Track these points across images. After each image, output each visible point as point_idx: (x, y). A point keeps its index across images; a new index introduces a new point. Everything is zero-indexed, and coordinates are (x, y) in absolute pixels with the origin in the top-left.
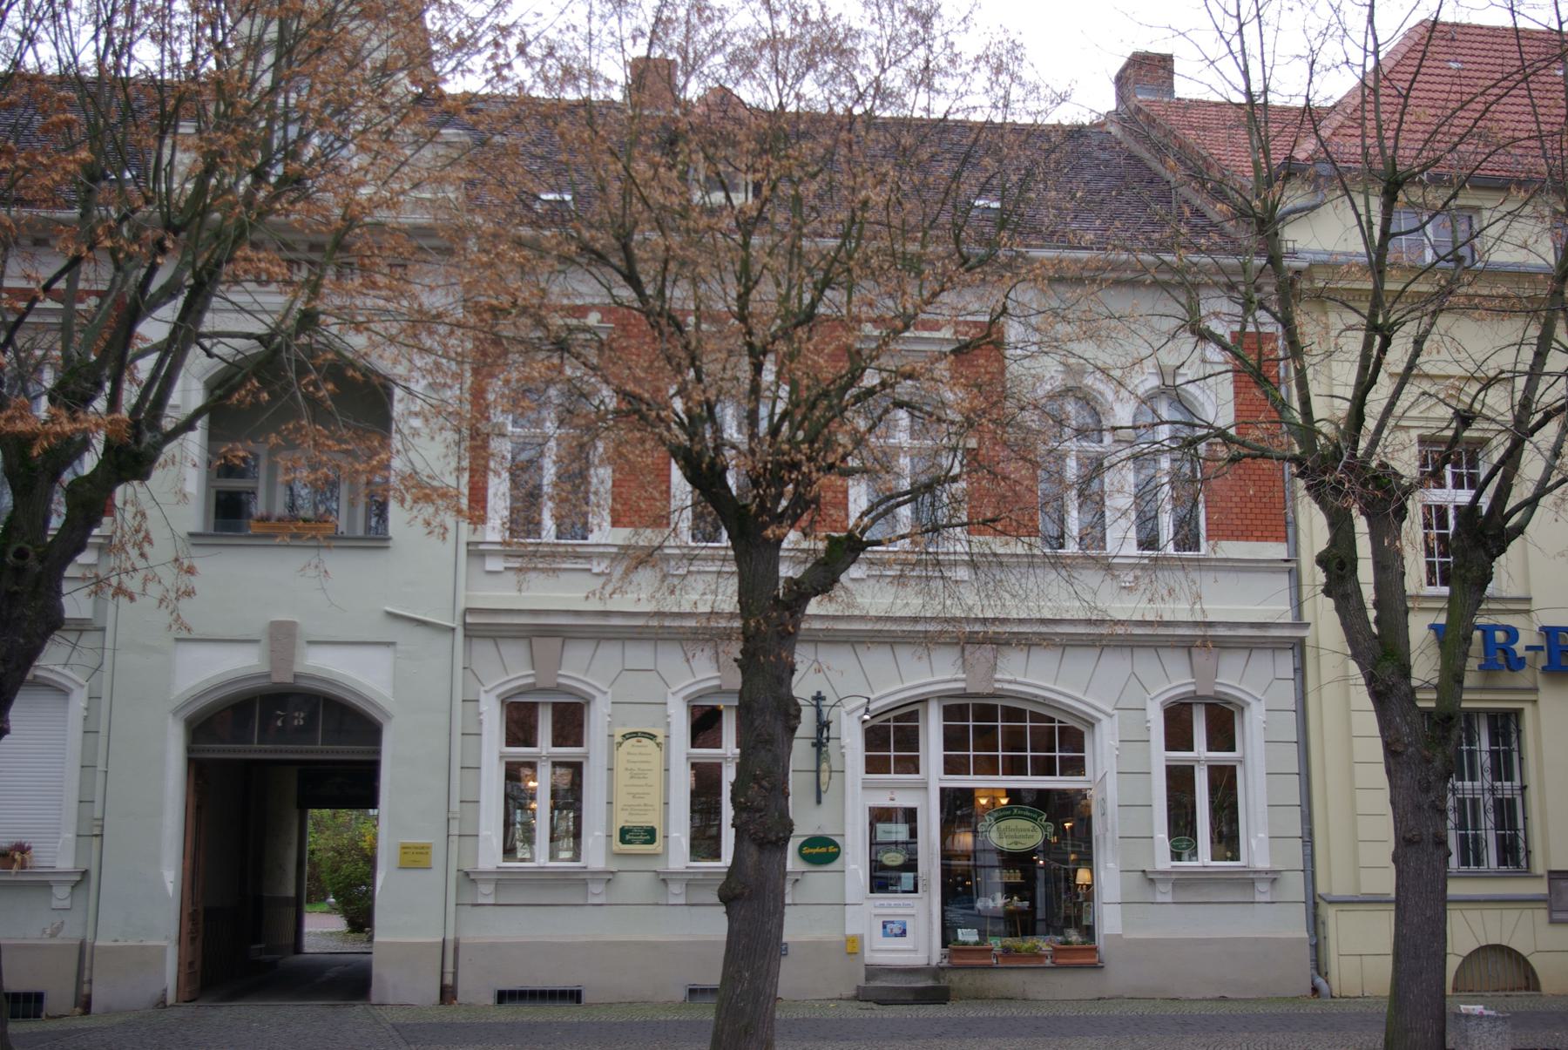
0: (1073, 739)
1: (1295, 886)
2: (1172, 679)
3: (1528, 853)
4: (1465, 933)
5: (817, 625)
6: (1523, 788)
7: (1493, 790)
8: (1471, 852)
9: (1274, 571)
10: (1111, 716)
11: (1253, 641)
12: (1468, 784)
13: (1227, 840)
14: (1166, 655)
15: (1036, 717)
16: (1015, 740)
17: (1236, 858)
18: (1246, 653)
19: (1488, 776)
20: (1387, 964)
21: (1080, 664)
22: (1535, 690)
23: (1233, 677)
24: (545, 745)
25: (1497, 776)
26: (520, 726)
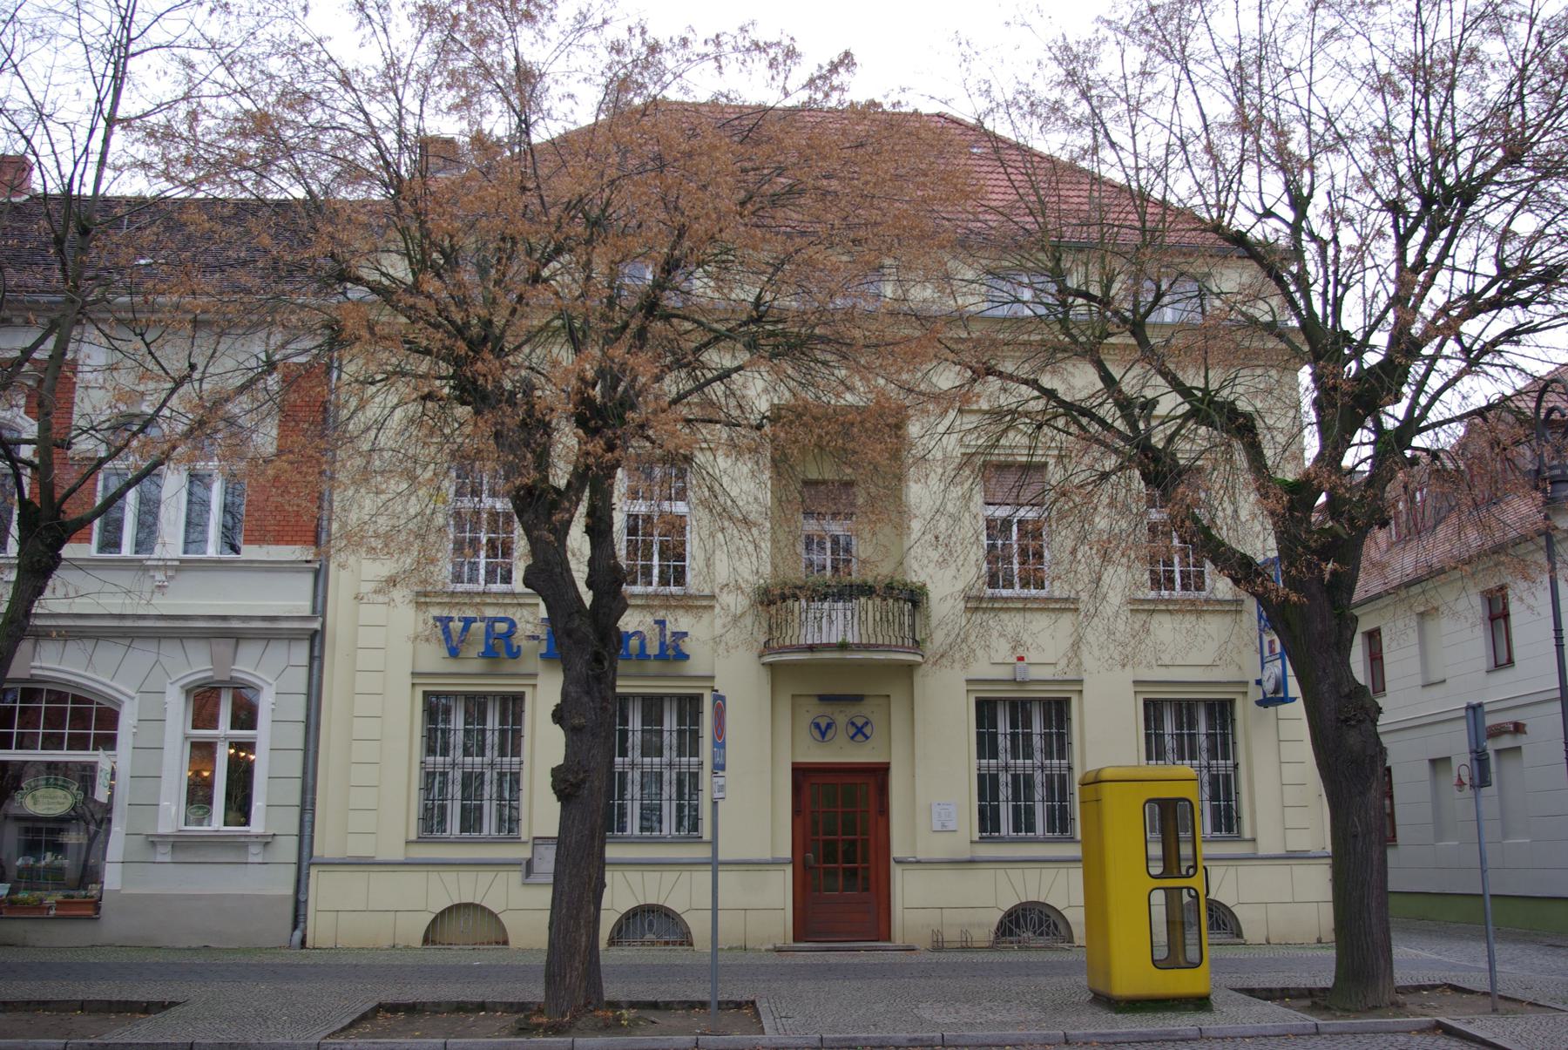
0: (109, 718)
1: (287, 849)
2: (198, 664)
3: (1239, 818)
4: (621, 893)
5: (38, 622)
6: (1236, 766)
7: (1209, 767)
8: (651, 817)
9: (298, 571)
10: (132, 698)
11: (269, 632)
12: (1221, 762)
13: (240, 804)
14: (191, 645)
15: (76, 699)
16: (55, 719)
17: (247, 823)
18: (264, 643)
19: (1205, 755)
20: (1327, 913)
21: (109, 653)
22: (535, 676)
23: (249, 665)
24: (224, 728)
25: (1213, 754)
26: (203, 714)
